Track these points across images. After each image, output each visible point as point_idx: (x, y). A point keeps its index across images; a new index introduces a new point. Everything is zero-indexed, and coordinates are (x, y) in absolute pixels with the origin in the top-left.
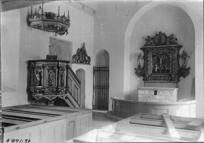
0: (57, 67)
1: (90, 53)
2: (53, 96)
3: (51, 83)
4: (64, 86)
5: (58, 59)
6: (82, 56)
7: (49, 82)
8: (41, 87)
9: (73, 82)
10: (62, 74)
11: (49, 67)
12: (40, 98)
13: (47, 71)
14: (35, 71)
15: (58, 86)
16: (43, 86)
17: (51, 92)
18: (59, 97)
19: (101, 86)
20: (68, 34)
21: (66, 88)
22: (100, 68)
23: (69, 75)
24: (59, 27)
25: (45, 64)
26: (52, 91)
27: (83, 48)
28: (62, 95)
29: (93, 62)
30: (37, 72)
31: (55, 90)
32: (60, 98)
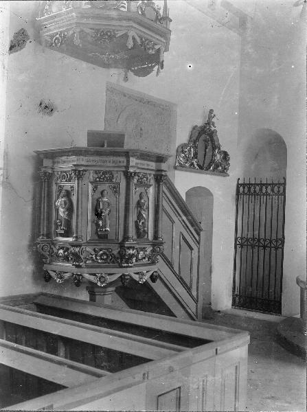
0: (124, 175)
1: (229, 137)
2: (113, 270)
3: (102, 228)
4: (146, 237)
5: (126, 147)
6: (205, 149)
7: (97, 225)
8: (70, 239)
9: (178, 228)
10: (141, 197)
11: (96, 172)
12: (67, 276)
13: (90, 187)
14: (54, 188)
15: (126, 238)
16: (76, 237)
17: (101, 259)
18: (128, 275)
19: (259, 240)
20: (162, 67)
21: (154, 245)
22: (246, 187)
23: (165, 204)
24: (134, 39)
25: (83, 163)
26: (104, 253)
27: (208, 124)
28: (137, 269)
29: (237, 171)
30: (60, 188)
31: (115, 252)
32: (132, 280)
